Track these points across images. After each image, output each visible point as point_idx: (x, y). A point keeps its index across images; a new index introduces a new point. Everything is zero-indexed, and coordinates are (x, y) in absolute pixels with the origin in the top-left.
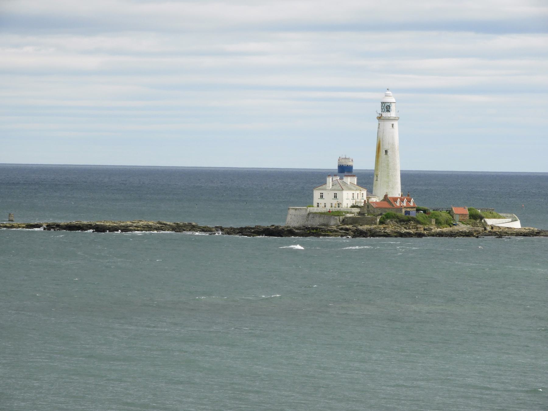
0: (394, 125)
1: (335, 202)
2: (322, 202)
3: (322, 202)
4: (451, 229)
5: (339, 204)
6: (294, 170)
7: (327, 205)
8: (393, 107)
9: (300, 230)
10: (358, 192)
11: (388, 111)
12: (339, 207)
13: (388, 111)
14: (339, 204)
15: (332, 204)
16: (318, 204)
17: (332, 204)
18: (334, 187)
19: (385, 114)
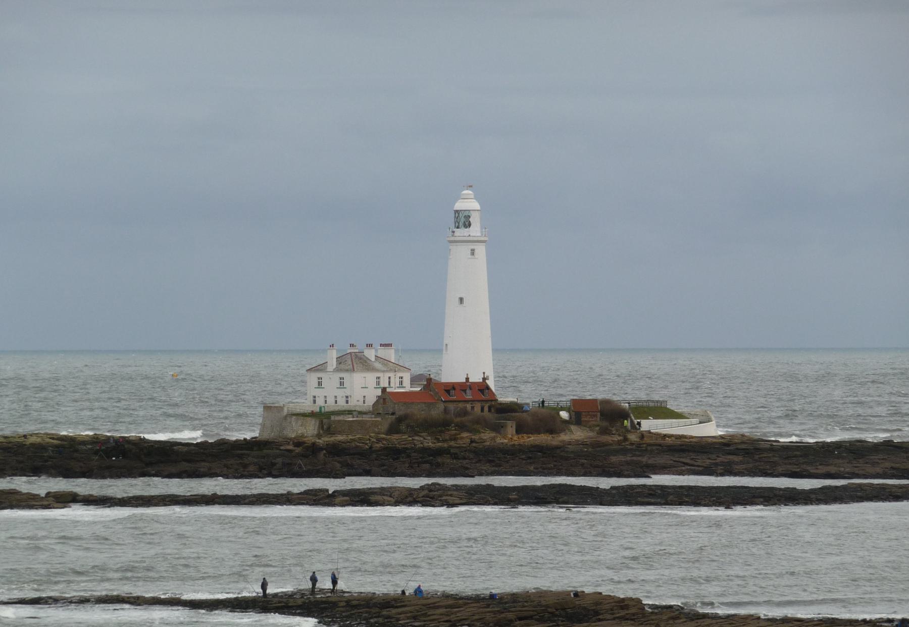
0: (476, 252)
1: (341, 393)
2: (320, 393)
3: (320, 393)
4: (332, 439)
5: (347, 397)
6: (710, 440)
7: (338, 400)
8: (475, 220)
9: (53, 439)
10: (391, 375)
11: (468, 225)
12: (347, 402)
13: (468, 225)
14: (347, 397)
15: (336, 397)
16: (315, 397)
17: (336, 397)
18: (342, 366)
19: (461, 233)
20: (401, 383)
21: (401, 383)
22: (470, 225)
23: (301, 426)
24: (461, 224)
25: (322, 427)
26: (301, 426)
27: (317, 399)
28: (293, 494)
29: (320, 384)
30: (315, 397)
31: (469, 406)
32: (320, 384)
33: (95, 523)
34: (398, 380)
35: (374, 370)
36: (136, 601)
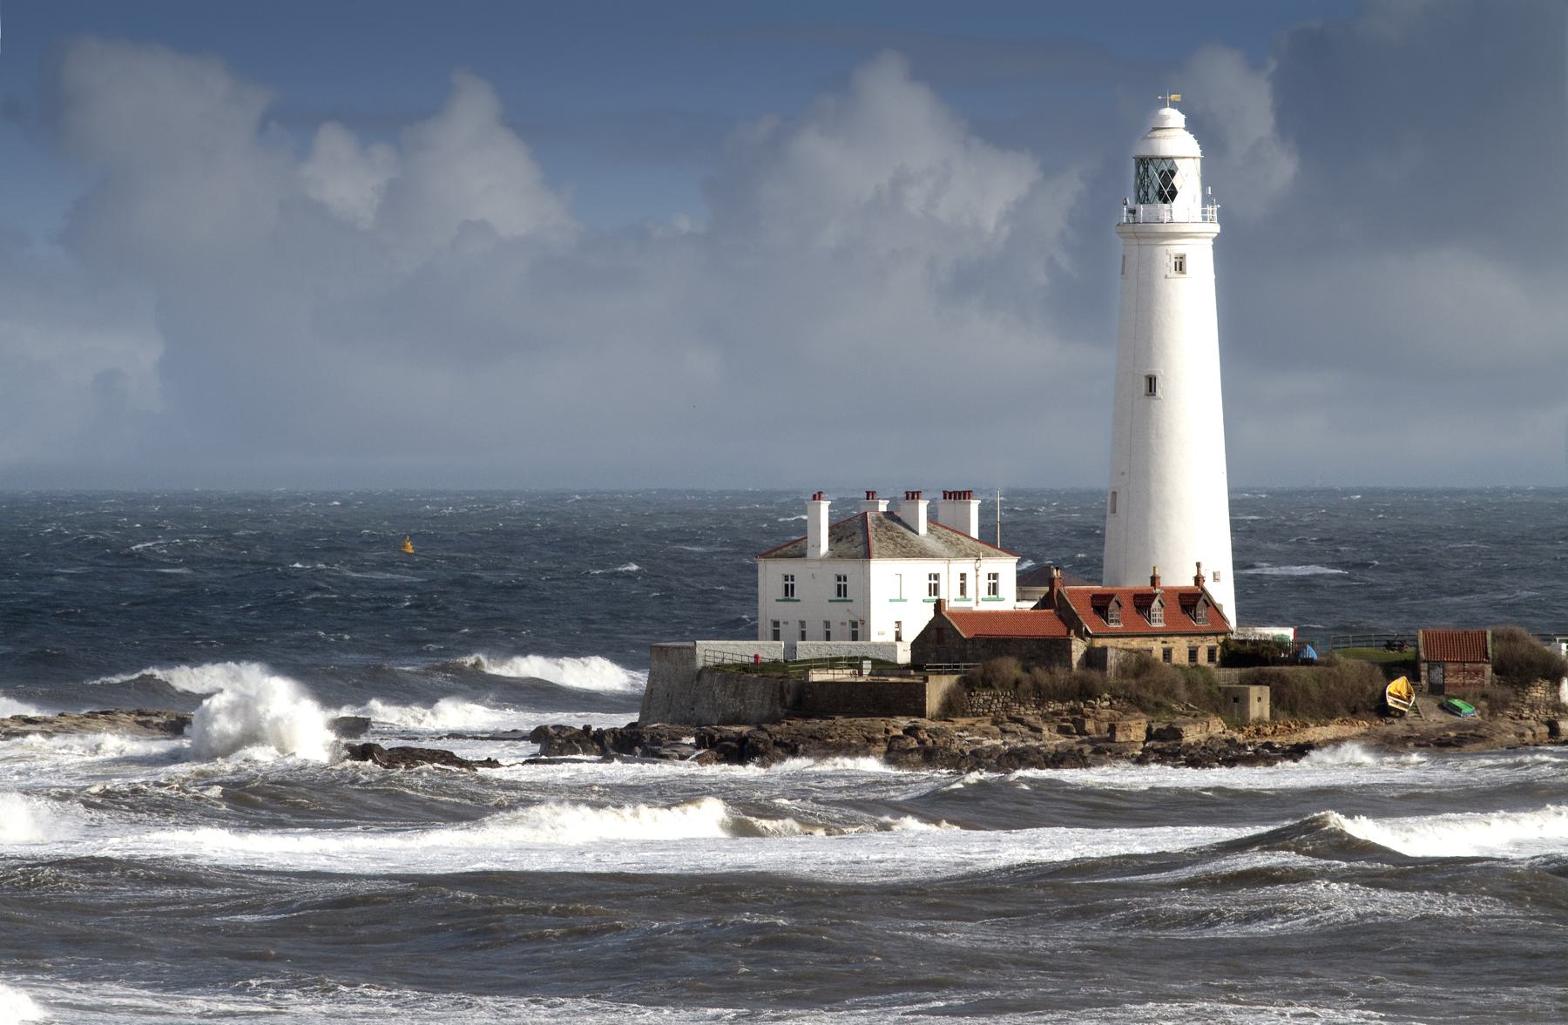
5: (854, 624)
10: (967, 565)
14: (854, 624)
16: (776, 624)
20: (994, 589)
21: (994, 589)
22: (1173, 194)
23: (734, 695)
24: (1151, 193)
25: (782, 698)
26: (734, 695)
27: (782, 627)
28: (1157, 761)
29: (789, 590)
30: (776, 624)
31: (1157, 647)
32: (789, 590)
33: (511, 807)
34: (984, 584)
35: (923, 554)
36: (79, 1007)
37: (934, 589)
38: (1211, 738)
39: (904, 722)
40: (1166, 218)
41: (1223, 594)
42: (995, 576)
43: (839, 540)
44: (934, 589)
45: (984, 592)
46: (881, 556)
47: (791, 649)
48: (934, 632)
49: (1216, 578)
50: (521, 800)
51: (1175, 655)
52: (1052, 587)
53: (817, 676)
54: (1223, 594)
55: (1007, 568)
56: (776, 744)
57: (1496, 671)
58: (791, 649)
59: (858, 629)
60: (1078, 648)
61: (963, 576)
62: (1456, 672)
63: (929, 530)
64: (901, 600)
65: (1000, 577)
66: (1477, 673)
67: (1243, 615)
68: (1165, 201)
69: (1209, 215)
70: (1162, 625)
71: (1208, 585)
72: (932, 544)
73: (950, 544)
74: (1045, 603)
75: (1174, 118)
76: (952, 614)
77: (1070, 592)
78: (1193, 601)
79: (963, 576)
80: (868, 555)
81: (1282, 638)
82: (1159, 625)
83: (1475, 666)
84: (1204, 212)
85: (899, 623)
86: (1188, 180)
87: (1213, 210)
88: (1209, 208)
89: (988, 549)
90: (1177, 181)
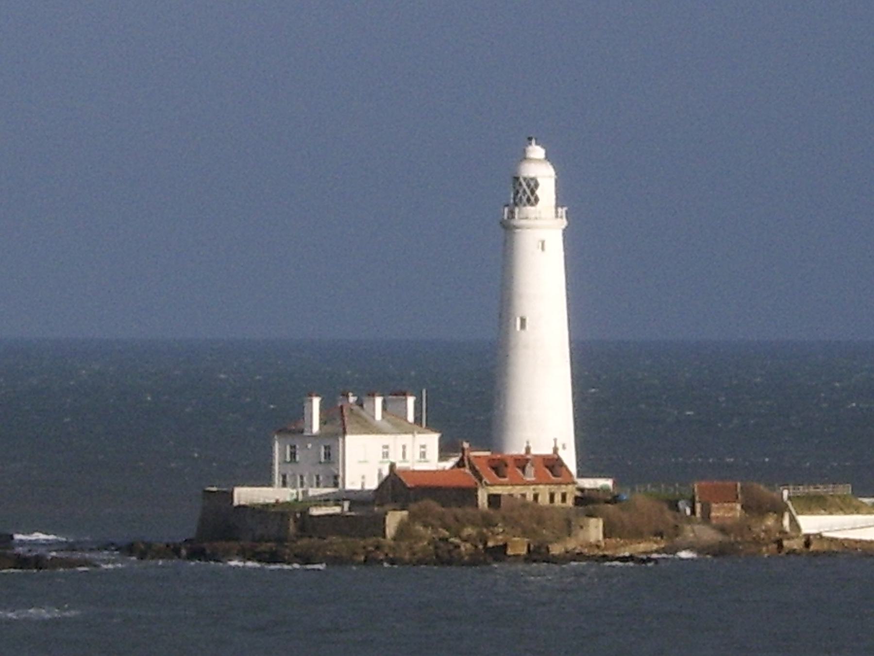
10: (406, 439)
20: (423, 455)
21: (423, 455)
22: (537, 200)
37: (386, 455)
38: (567, 552)
39: (371, 540)
40: (533, 216)
41: (569, 459)
42: (423, 447)
43: (325, 423)
44: (386, 455)
45: (417, 457)
46: (352, 433)
47: (305, 493)
48: (389, 483)
49: (564, 447)
50: (627, 561)
51: (540, 498)
52: (463, 454)
53: (315, 512)
54: (569, 459)
55: (432, 440)
56: (296, 556)
57: (742, 507)
58: (305, 493)
59: (335, 480)
60: (482, 497)
61: (404, 447)
62: (718, 509)
63: (383, 417)
64: (365, 462)
65: (428, 447)
66: (732, 509)
67: (581, 475)
68: (532, 205)
69: (559, 214)
70: (533, 479)
71: (562, 454)
72: (386, 425)
73: (395, 425)
74: (460, 464)
75: (537, 152)
76: (399, 471)
77: (476, 457)
78: (553, 464)
79: (404, 447)
80: (344, 433)
81: (606, 486)
82: (531, 479)
83: (730, 505)
84: (557, 212)
85: (363, 477)
86: (547, 190)
87: (562, 211)
88: (560, 210)
89: (417, 427)
90: (538, 192)
